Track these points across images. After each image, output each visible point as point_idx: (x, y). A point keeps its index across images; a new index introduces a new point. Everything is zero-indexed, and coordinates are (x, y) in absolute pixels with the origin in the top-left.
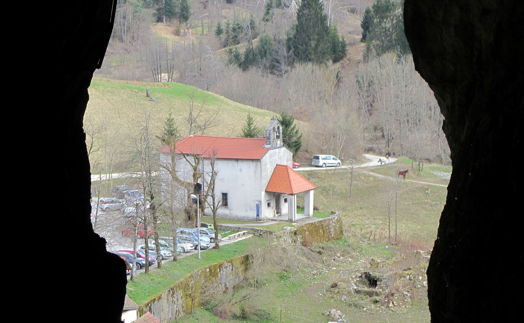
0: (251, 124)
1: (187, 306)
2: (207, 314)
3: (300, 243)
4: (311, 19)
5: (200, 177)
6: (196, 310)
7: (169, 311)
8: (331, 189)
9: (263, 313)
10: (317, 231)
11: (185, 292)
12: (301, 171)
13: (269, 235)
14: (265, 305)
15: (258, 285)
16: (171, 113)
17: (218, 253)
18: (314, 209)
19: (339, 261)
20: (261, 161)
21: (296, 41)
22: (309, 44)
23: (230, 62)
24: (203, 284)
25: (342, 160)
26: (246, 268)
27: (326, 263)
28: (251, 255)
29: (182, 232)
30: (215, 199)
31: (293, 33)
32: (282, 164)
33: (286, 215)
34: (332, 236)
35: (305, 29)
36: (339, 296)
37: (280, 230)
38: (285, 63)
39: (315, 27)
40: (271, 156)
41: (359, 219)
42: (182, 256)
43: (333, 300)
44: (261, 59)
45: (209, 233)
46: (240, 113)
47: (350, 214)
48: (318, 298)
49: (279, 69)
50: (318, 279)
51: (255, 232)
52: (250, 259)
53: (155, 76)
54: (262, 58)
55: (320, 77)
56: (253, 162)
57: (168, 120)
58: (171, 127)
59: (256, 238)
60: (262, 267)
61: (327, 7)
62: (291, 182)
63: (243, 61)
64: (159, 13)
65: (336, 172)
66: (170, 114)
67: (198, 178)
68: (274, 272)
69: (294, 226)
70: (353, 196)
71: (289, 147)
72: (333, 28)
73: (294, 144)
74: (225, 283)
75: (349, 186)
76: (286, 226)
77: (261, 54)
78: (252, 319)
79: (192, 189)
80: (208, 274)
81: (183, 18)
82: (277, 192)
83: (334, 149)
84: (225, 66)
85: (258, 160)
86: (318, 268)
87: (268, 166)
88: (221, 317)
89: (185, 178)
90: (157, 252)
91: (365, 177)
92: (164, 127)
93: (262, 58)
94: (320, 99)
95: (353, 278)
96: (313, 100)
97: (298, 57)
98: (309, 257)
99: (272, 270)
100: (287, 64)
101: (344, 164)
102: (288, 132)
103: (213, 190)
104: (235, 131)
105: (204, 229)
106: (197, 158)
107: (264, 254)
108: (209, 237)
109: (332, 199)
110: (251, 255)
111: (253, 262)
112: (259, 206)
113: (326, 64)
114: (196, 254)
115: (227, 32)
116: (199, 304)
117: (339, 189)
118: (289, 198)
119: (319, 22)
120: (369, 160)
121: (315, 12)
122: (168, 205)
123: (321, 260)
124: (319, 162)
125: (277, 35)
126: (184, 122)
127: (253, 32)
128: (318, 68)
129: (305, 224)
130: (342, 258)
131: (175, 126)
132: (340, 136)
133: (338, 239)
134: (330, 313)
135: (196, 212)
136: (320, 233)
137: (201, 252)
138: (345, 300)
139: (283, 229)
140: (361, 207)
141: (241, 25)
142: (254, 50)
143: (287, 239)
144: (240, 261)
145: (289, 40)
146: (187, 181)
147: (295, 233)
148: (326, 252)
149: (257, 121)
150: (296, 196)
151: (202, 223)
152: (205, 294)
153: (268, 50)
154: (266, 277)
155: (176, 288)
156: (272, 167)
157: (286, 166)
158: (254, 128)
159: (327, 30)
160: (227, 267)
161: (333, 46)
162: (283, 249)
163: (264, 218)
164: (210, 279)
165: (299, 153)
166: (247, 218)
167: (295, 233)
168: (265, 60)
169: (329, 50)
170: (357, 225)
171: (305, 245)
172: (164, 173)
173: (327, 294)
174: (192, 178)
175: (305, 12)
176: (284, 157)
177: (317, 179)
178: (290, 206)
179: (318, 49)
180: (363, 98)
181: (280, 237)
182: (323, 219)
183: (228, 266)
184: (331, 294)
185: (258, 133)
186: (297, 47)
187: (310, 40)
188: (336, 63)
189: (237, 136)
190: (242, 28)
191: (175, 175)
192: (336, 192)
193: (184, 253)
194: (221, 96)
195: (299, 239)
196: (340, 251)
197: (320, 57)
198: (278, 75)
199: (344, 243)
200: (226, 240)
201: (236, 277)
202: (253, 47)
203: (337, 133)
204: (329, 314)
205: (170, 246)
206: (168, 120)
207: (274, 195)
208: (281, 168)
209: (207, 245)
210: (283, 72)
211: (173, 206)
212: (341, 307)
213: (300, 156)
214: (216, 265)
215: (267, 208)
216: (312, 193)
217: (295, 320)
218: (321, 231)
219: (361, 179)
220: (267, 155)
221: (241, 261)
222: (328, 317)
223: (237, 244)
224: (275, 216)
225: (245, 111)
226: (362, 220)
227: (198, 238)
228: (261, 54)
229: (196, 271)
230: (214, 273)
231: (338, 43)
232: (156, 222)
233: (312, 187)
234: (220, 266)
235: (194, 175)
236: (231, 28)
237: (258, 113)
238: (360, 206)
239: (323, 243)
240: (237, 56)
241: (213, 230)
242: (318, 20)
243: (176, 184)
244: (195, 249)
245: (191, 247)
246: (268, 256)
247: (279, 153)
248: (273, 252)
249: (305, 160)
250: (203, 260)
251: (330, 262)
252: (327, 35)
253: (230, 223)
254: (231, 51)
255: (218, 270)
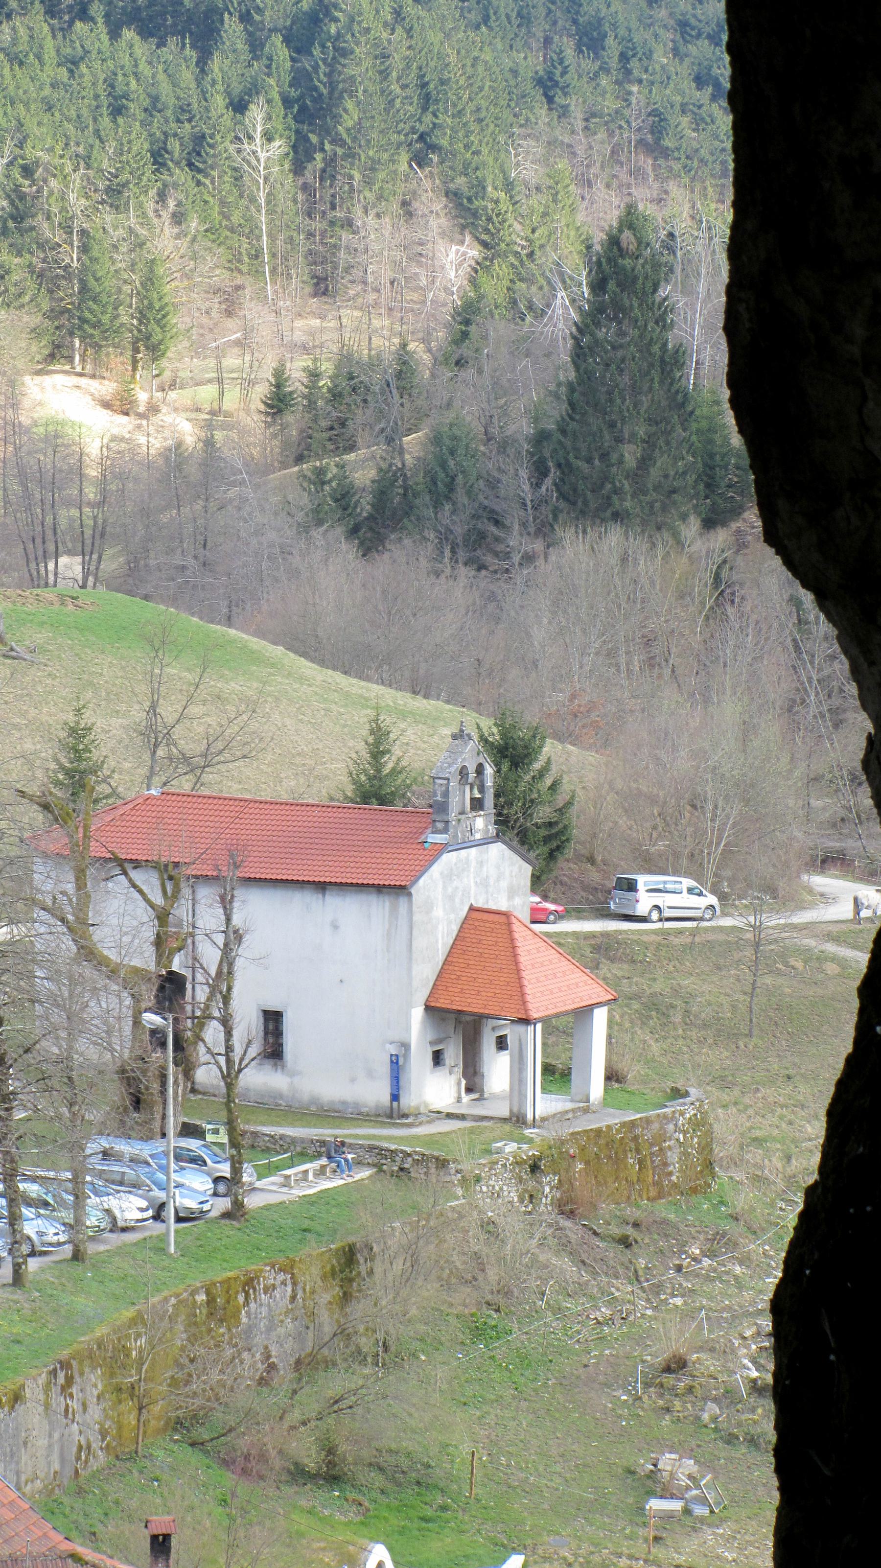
0: (383, 753)
1: (120, 1428)
2: (193, 1460)
3: (552, 1204)
4: (623, 360)
5: (180, 950)
6: (152, 1444)
7: (50, 1446)
8: (678, 1003)
9: (404, 1463)
10: (618, 1161)
11: (112, 1375)
12: (567, 934)
13: (433, 1170)
14: (413, 1431)
15: (387, 1358)
16: (84, 707)
17: (240, 1234)
18: (608, 1078)
19: (697, 1276)
20: (410, 895)
21: (568, 443)
22: (614, 457)
23: (318, 517)
24: (183, 1349)
25: (722, 897)
26: (345, 1293)
27: (647, 1280)
28: (366, 1246)
29: (106, 1154)
30: (236, 1033)
31: (557, 411)
32: (492, 906)
33: (504, 1098)
34: (674, 1178)
35: (603, 398)
36: (694, 1404)
37: (477, 1151)
38: (524, 525)
39: (639, 394)
40: (449, 877)
41: (781, 1117)
42: (104, 1242)
43: (667, 1417)
44: (435, 507)
45: (208, 1161)
46: (342, 710)
47: (747, 1100)
48: (613, 1410)
49: (500, 547)
50: (617, 1339)
51: (384, 1161)
52: (362, 1261)
53: (33, 565)
54: (437, 505)
55: (653, 583)
56: (381, 897)
57: (73, 731)
58: (79, 759)
59: (386, 1182)
60: (404, 1293)
61: (685, 318)
62: (524, 974)
63: (365, 514)
64: (57, 328)
65: (697, 939)
66: (79, 710)
67: (171, 954)
68: (450, 1310)
69: (530, 1141)
70: (762, 1030)
71: (522, 843)
72: (706, 395)
73: (543, 832)
74: (266, 1348)
75: (745, 994)
76: (502, 1139)
77: (434, 489)
78: (364, 1483)
79: (149, 996)
80: (202, 1313)
81: (147, 348)
82: (470, 1009)
83: (692, 855)
84: (299, 533)
85: (401, 890)
86: (615, 1299)
87: (439, 912)
88: (245, 1472)
89: (123, 952)
90: (12, 1225)
91: (805, 962)
92: (57, 761)
93: (437, 505)
94: (652, 666)
95: (744, 1338)
96: (623, 667)
97: (574, 503)
98: (584, 1257)
99: (444, 1302)
100: (532, 530)
101: (731, 910)
102: (522, 786)
103: (226, 999)
104: (322, 778)
105: (193, 1144)
106: (171, 878)
107: (416, 1243)
108: (209, 1174)
109: (681, 1042)
110: (366, 1246)
111: (371, 1273)
112: (401, 1062)
113: (676, 535)
114: (158, 1237)
115: (311, 404)
116: (167, 1424)
117: (710, 1005)
118: (510, 1031)
119: (655, 374)
120: (826, 898)
121: (641, 336)
122: (56, 1050)
123: (627, 1268)
124: (637, 901)
125: (495, 420)
126: (131, 738)
127: (407, 404)
128: (645, 546)
129: (572, 1134)
130: (706, 1262)
131: (96, 755)
132: (716, 807)
133: (694, 1190)
134: (655, 1465)
135: (163, 1078)
136: (626, 1167)
137: (176, 1231)
138: (714, 1419)
139: (488, 1152)
140: (791, 1072)
141: (363, 378)
142: (409, 474)
143: (501, 1189)
144: (323, 1267)
145: (541, 437)
146: (132, 964)
147: (534, 1168)
148: (647, 1241)
149: (407, 744)
150: (539, 1026)
151: (186, 1120)
152: (187, 1389)
153: (460, 476)
154: (422, 1328)
155: (81, 1363)
156: (452, 916)
157: (506, 915)
158: (393, 769)
159: (683, 405)
160: (274, 1287)
161: (705, 465)
162: (488, 1224)
163: (418, 1108)
164: (210, 1330)
165: (565, 867)
166: (356, 1105)
167: (534, 1168)
168: (447, 514)
169: (691, 478)
170: (774, 1139)
171: (572, 1212)
172: (42, 930)
173: (645, 1398)
174: (152, 949)
175: (601, 333)
176: (498, 880)
177: (625, 966)
178: (516, 1066)
179: (648, 473)
180: (812, 663)
181: (478, 1179)
182: (638, 1116)
183: (278, 1283)
184: (661, 1396)
185: (409, 787)
186: (569, 464)
187: (619, 440)
188: (712, 531)
189: (332, 799)
190: (367, 389)
191: (86, 936)
192: (696, 1016)
193: (111, 1231)
194: (275, 643)
195: (548, 1185)
196: (702, 1237)
197: (657, 505)
198: (496, 572)
199: (715, 1207)
200: (274, 1188)
201: (308, 1328)
202: (404, 465)
203: (706, 792)
204: (652, 1471)
205: (62, 1203)
206: (73, 731)
207: (458, 1022)
208: (483, 921)
209: (201, 1203)
210: (516, 559)
211: (76, 1057)
212: (699, 1446)
213: (565, 879)
214: (232, 1281)
215: (432, 1072)
216: (600, 1016)
217: (524, 1491)
218: (631, 1161)
219: (793, 968)
220: (436, 870)
221: (328, 1267)
222: (649, 1483)
223: (312, 1204)
224: (459, 1100)
225: (363, 702)
226: (790, 1123)
227: (169, 1179)
228: (434, 489)
229: (155, 1299)
230: (225, 1309)
231: (724, 456)
232: (10, 1115)
233: (603, 993)
234: (246, 1283)
235: (159, 942)
236: (325, 390)
237: (411, 712)
238: (787, 1069)
239: (638, 1207)
240: (343, 496)
241: (224, 1150)
242: (652, 365)
243: (87, 970)
244: (157, 1217)
245: (142, 1210)
246: (428, 1251)
247: (481, 864)
248: (448, 1237)
249: (584, 894)
250: (185, 1259)
251: (663, 1275)
252: (682, 424)
253: (292, 1125)
254: (319, 478)
255: (241, 1298)
